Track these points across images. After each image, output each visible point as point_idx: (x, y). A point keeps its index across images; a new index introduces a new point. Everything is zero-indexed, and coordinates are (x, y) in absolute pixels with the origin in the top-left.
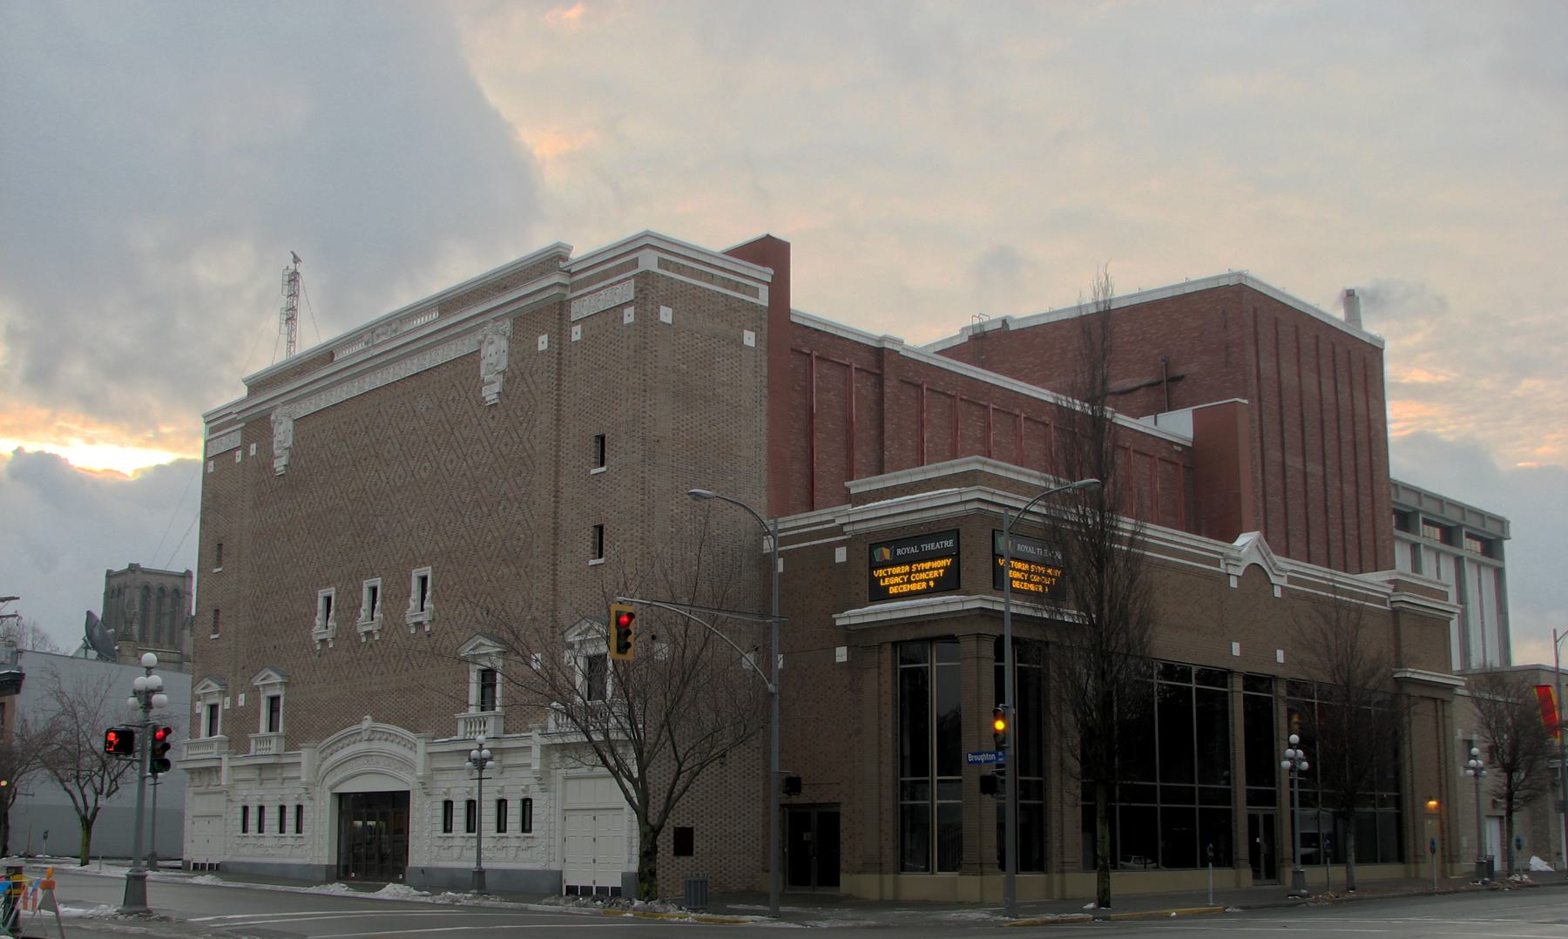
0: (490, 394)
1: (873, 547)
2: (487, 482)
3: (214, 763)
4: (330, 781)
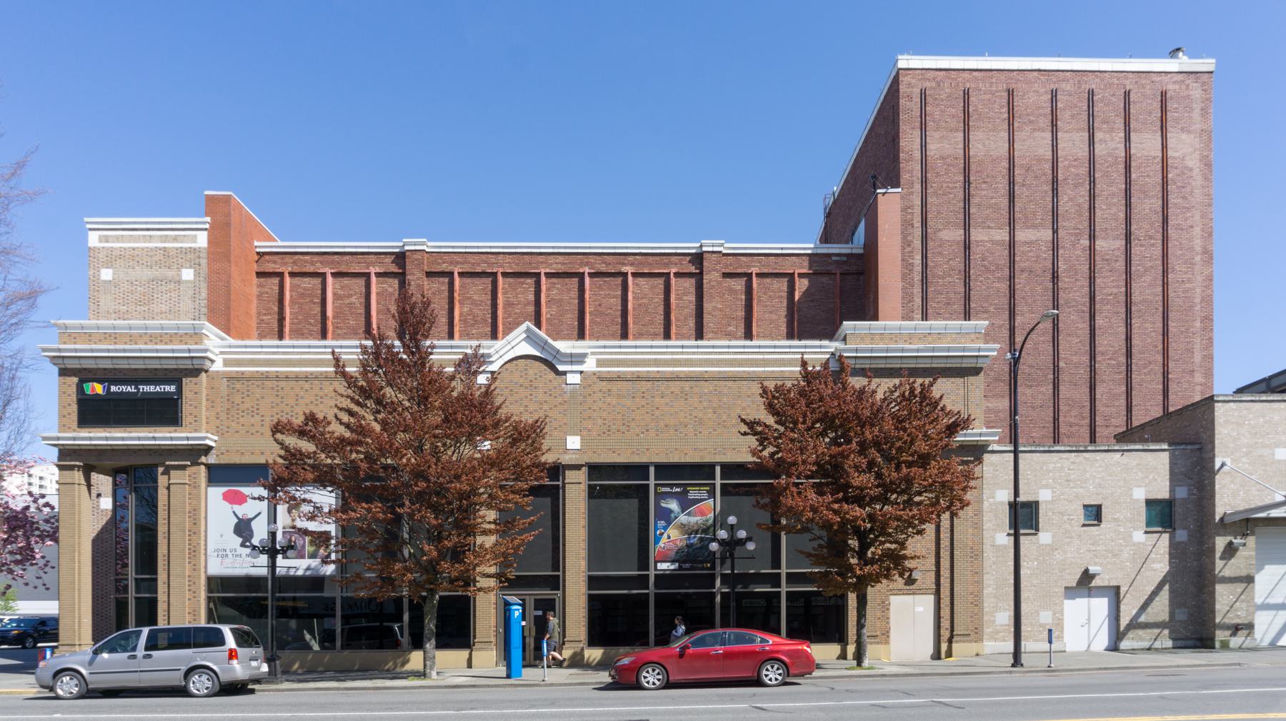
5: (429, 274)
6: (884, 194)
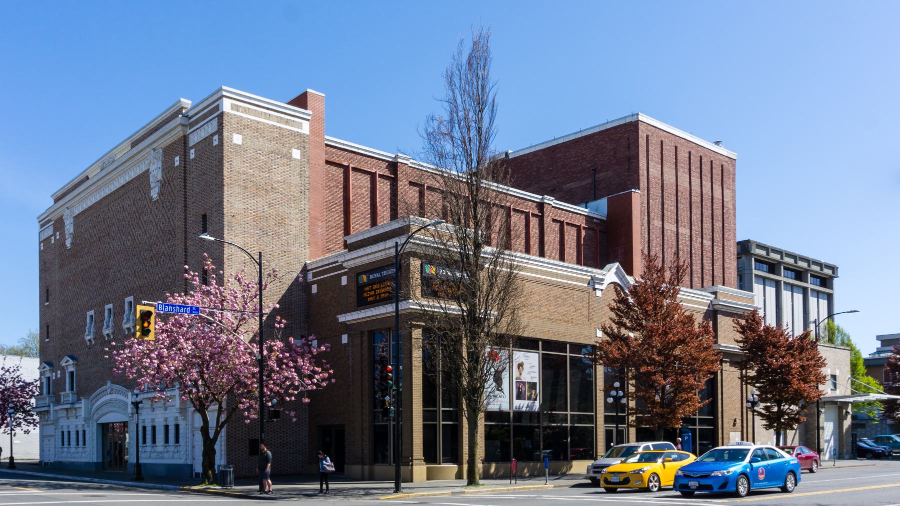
0: (154, 194)
1: (359, 274)
2: (155, 246)
3: (46, 409)
4: (95, 417)
5: (411, 183)
6: (634, 192)
